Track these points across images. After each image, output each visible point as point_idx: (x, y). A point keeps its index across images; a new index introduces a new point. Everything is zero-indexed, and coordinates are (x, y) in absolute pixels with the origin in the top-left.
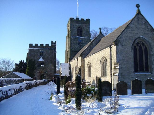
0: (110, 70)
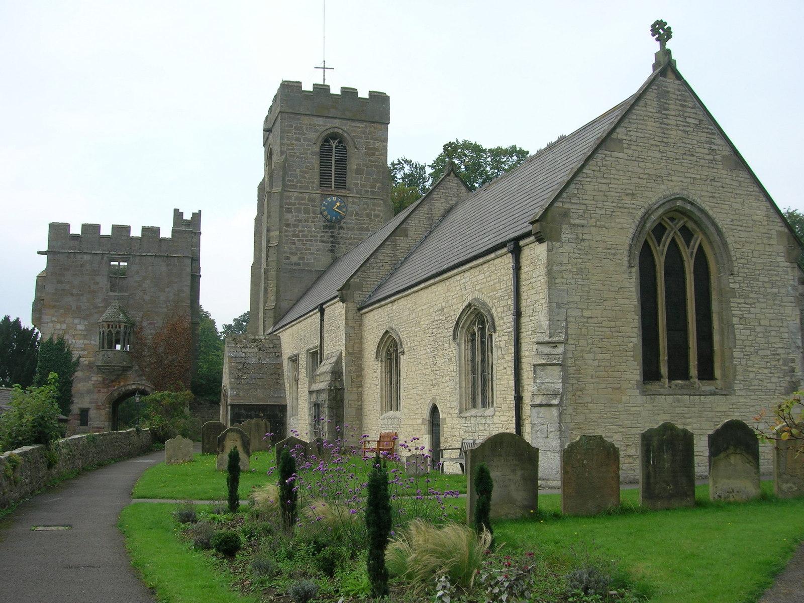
0: (511, 371)
